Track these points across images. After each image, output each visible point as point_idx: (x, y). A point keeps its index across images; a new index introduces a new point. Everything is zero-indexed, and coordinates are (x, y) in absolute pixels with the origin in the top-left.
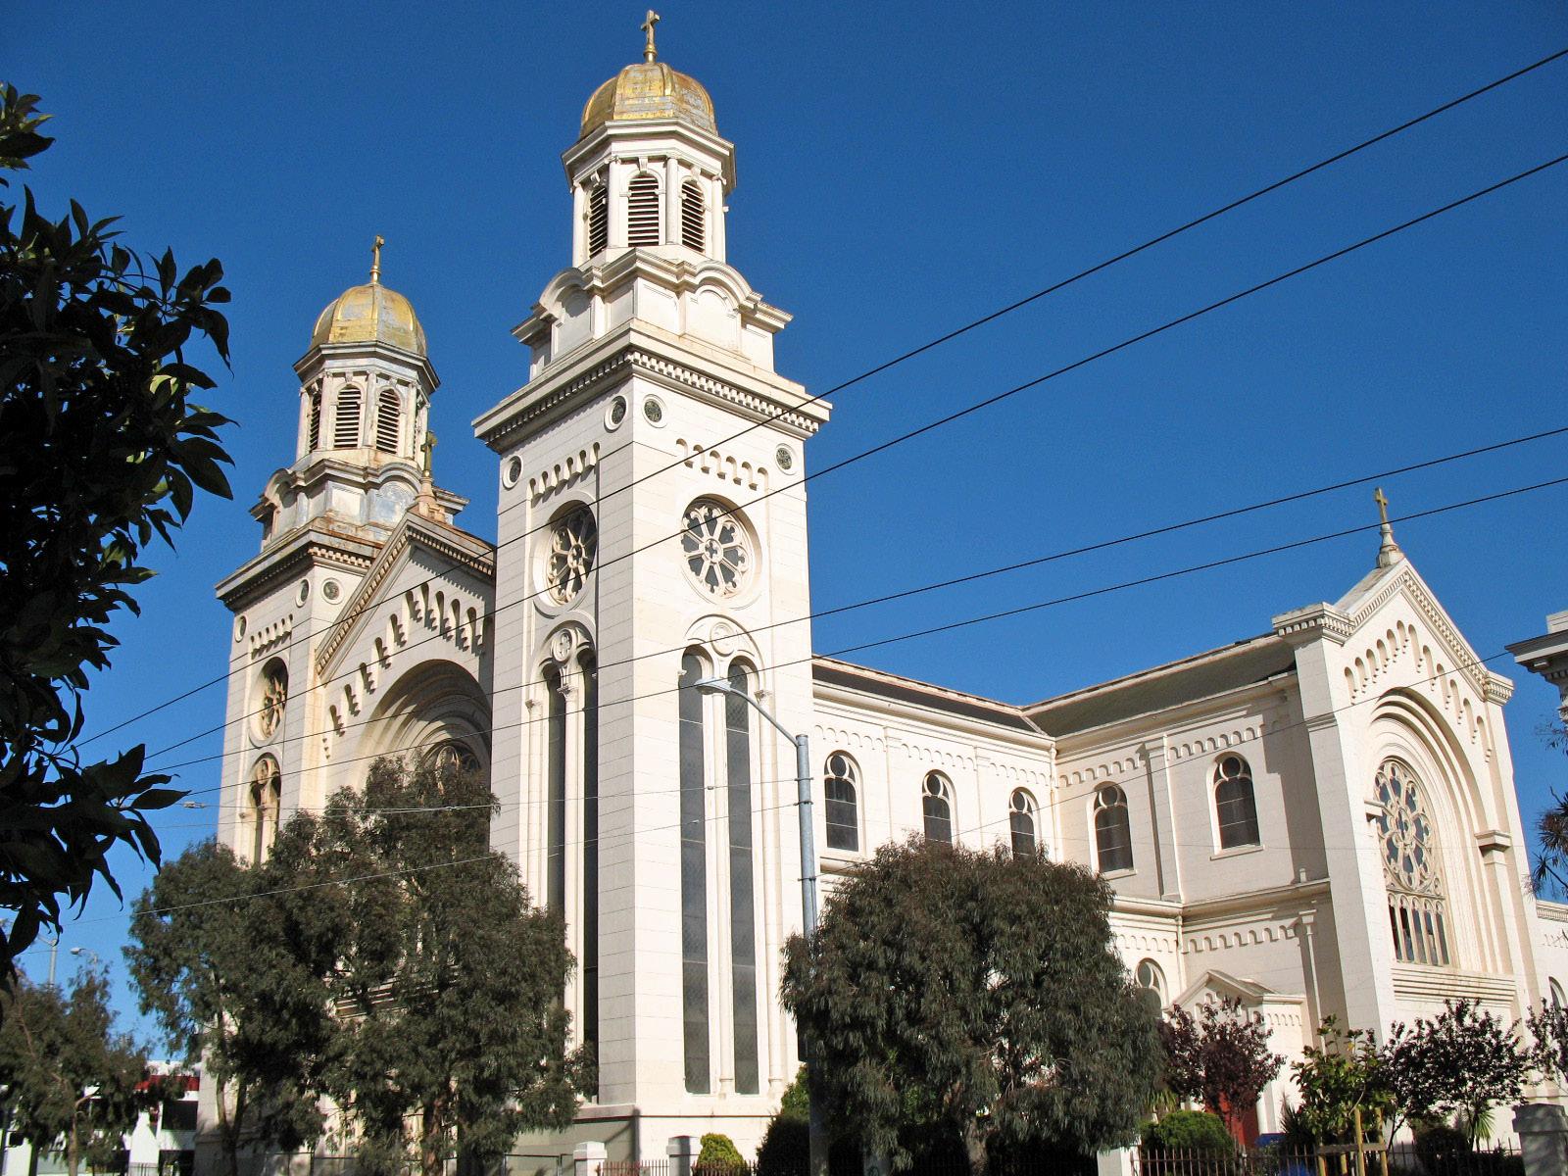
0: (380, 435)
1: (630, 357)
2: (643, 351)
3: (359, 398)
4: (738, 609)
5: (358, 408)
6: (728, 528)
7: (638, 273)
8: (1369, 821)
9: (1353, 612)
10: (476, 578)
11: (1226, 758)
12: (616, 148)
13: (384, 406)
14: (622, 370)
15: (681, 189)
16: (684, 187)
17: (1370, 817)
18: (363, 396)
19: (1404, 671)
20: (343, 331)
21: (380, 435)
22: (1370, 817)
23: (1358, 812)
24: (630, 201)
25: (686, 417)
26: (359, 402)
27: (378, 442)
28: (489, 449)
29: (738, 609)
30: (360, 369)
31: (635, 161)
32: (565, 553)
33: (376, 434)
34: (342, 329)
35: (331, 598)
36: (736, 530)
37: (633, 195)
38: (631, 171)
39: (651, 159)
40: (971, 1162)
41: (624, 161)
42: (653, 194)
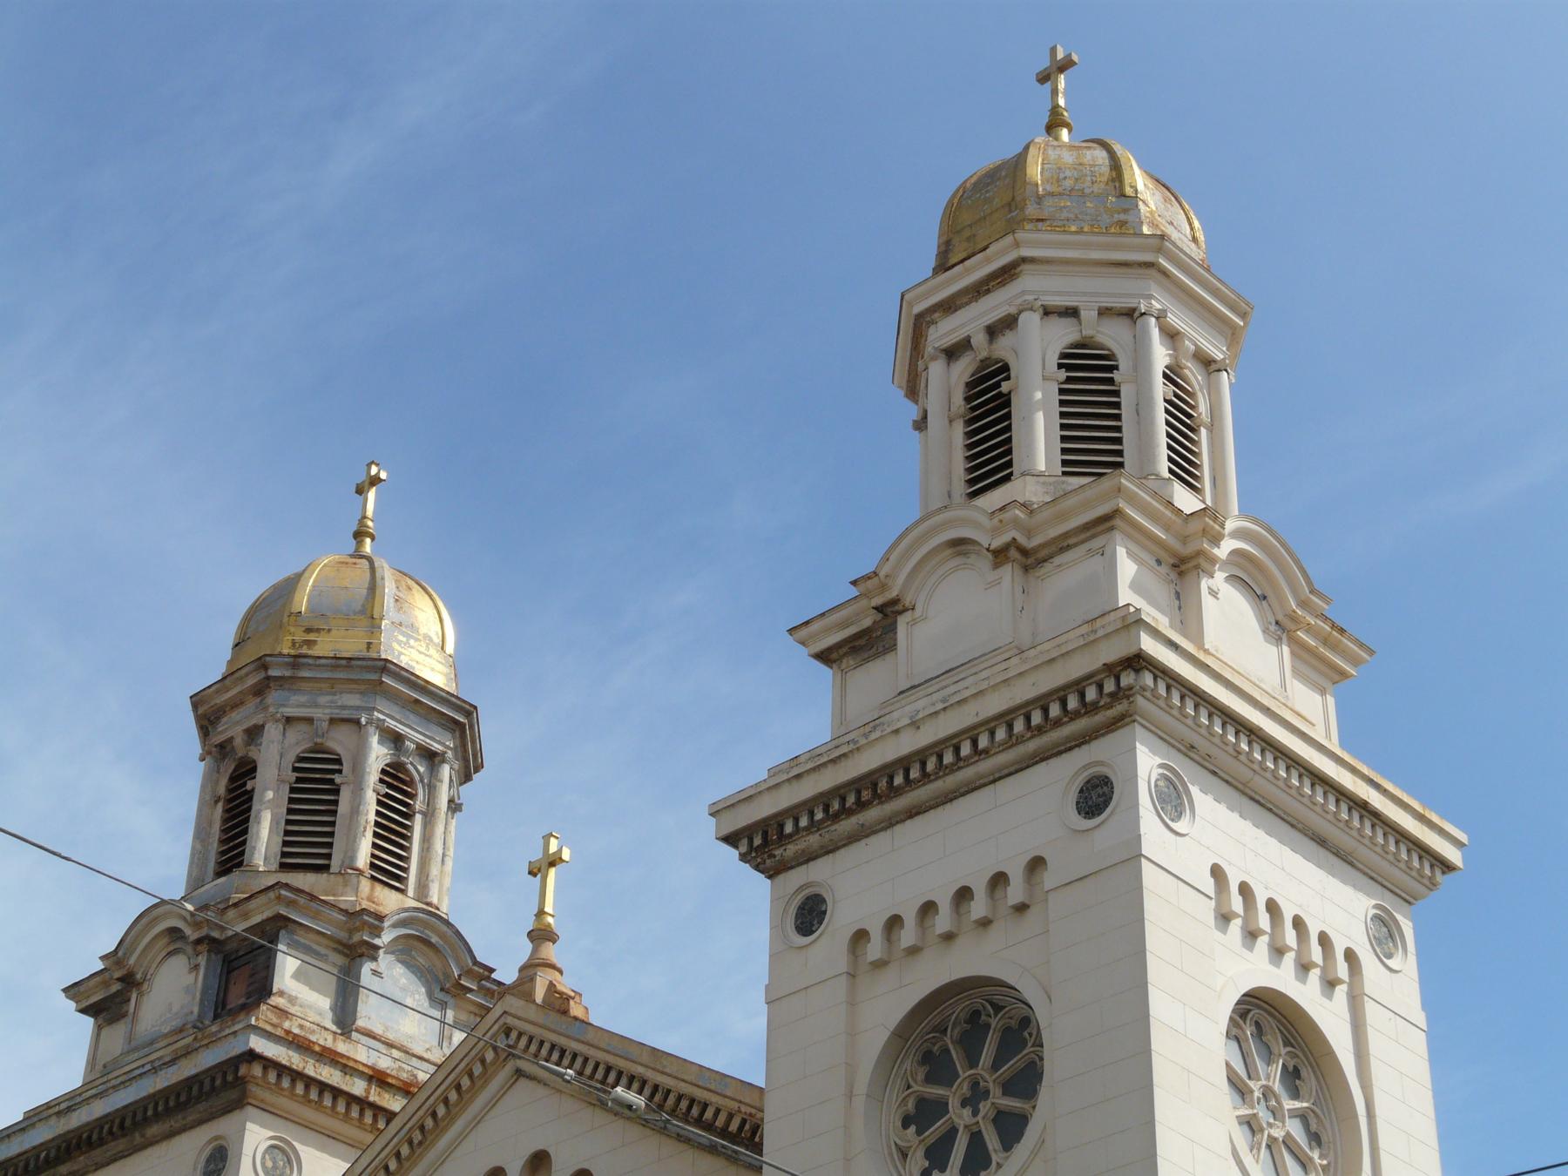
0: (377, 853)
1: (1127, 679)
2: (1161, 672)
3: (340, 771)
5: (337, 792)
6: (913, 1129)
7: (1117, 522)
12: (1030, 284)
13: (387, 795)
14: (1109, 706)
18: (346, 768)
20: (311, 637)
21: (377, 853)
24: (1062, 391)
28: (732, 854)
30: (346, 714)
31: (1072, 313)
32: (937, 1091)
34: (309, 630)
36: (1304, 1073)
38: (1062, 335)
39: (1104, 312)
41: (1047, 312)
42: (331, 781)
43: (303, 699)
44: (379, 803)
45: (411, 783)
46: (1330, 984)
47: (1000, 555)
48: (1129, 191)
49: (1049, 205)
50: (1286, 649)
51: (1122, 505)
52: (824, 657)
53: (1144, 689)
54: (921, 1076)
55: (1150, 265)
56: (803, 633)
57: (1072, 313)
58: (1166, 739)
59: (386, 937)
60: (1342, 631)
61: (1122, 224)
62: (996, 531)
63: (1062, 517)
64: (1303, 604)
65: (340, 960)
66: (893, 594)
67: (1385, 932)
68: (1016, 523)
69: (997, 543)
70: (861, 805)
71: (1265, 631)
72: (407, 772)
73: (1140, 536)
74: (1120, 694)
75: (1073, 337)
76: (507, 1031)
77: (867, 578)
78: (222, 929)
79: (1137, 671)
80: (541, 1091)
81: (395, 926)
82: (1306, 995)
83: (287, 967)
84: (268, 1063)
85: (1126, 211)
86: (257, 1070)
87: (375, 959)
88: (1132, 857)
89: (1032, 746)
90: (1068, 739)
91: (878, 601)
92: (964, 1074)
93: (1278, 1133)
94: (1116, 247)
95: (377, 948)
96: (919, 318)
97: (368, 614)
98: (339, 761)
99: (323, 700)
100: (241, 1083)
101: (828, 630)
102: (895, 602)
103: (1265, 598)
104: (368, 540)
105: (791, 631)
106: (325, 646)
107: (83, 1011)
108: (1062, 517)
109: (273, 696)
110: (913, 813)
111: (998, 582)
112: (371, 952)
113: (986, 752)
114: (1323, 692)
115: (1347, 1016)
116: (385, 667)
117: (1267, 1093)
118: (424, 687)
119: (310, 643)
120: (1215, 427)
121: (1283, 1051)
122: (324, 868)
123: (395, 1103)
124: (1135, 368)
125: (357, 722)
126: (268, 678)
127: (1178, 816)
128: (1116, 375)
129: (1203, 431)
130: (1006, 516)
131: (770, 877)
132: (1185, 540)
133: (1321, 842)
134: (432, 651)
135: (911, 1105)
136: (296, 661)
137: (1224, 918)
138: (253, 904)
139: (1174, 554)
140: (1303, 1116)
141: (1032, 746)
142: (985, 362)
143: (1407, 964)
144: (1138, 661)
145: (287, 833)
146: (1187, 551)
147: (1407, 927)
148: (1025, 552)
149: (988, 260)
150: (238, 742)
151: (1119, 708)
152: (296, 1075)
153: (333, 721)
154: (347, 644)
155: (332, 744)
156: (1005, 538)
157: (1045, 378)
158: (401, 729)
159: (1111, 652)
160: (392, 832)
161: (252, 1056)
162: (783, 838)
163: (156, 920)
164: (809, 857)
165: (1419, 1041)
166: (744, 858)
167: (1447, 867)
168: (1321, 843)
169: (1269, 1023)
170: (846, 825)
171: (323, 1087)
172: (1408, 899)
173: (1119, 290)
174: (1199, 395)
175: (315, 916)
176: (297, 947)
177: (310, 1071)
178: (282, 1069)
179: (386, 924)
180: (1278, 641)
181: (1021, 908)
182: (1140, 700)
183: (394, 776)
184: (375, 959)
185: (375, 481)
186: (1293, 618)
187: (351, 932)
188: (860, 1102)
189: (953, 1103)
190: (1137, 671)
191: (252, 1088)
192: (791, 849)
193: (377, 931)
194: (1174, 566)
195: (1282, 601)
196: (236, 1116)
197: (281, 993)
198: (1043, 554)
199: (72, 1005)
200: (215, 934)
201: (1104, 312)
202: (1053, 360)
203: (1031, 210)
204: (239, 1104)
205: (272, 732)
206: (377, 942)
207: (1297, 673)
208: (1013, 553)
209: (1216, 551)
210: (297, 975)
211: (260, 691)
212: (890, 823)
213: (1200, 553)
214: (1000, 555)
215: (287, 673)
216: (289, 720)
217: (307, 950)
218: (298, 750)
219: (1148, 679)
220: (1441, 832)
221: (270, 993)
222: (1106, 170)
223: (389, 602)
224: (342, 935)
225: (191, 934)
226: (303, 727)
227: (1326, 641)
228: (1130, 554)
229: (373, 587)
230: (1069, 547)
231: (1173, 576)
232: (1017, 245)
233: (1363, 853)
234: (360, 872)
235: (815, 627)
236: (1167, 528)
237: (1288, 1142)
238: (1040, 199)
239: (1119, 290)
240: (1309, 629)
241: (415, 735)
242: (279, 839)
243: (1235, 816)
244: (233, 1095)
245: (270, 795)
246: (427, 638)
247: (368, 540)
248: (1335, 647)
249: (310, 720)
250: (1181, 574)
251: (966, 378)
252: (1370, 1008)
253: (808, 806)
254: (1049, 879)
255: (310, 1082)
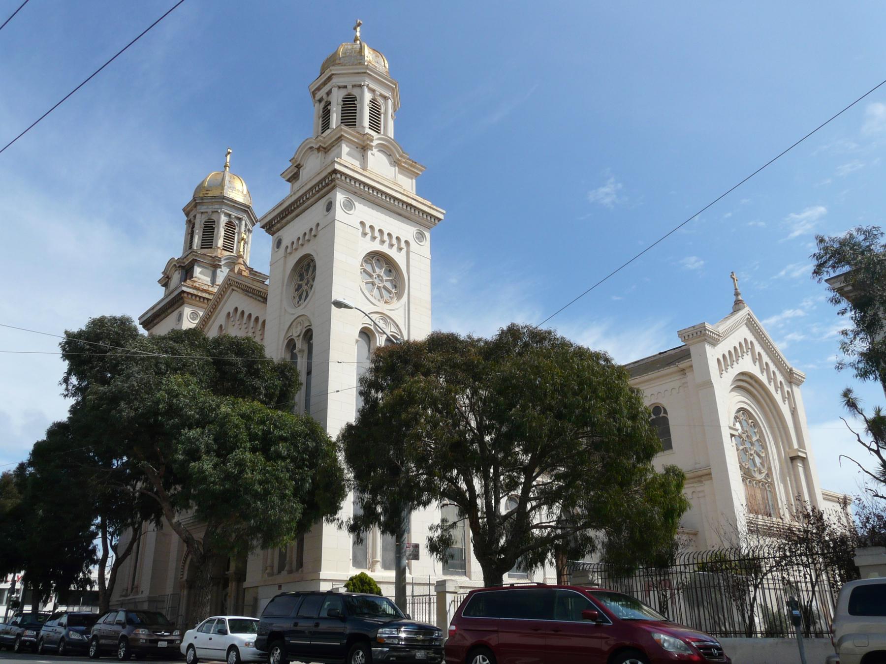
1: (334, 176)
2: (342, 174)
4: (390, 310)
5: (214, 229)
7: (342, 138)
8: (731, 438)
9: (721, 329)
10: (259, 300)
11: (654, 406)
12: (335, 81)
14: (331, 183)
15: (369, 102)
16: (370, 101)
17: (732, 435)
19: (746, 364)
22: (732, 435)
23: (726, 433)
25: (363, 212)
26: (214, 226)
27: (223, 246)
28: (263, 230)
29: (390, 310)
30: (215, 210)
31: (345, 87)
32: (301, 282)
33: (222, 242)
34: (207, 191)
35: (193, 320)
37: (344, 104)
38: (343, 93)
39: (354, 86)
40: (296, 540)
41: (339, 87)
42: (354, 104)
43: (205, 207)
44: (225, 231)
45: (234, 226)
46: (400, 249)
47: (318, 149)
48: (363, 54)
49: (342, 61)
50: (397, 168)
51: (343, 133)
52: (288, 180)
53: (338, 178)
54: (299, 279)
55: (365, 73)
56: (283, 175)
57: (345, 87)
58: (347, 190)
59: (223, 263)
60: (415, 163)
61: (360, 63)
62: (316, 145)
63: (331, 138)
64: (401, 156)
65: (212, 269)
66: (298, 163)
67: (420, 236)
68: (321, 141)
69: (317, 147)
70: (287, 215)
71: (391, 164)
72: (233, 223)
73: (349, 141)
74: (333, 180)
75: (346, 93)
76: (229, 280)
77: (292, 159)
78: (184, 263)
79: (336, 174)
80: (237, 293)
81: (225, 260)
82: (393, 253)
83: (197, 270)
84: (188, 293)
85: (361, 59)
86: (185, 295)
87: (221, 268)
88: (333, 220)
89: (317, 196)
90: (324, 193)
91: (295, 165)
92: (306, 277)
93: (381, 285)
94: (356, 69)
95: (221, 265)
96: (313, 92)
97: (222, 185)
98: (214, 222)
99: (210, 207)
100: (182, 298)
101: (288, 174)
102: (299, 164)
103: (390, 155)
104: (228, 168)
105: (281, 175)
106: (211, 194)
107: (162, 286)
108: (331, 138)
109: (198, 207)
110: (297, 216)
111: (318, 157)
112: (220, 266)
113: (308, 198)
114: (412, 179)
115: (405, 257)
116: (224, 198)
117: (379, 276)
118: (235, 202)
119: (207, 194)
120: (386, 113)
121: (385, 266)
122: (211, 248)
123: (211, 297)
124: (360, 100)
125: (218, 212)
126: (196, 203)
127: (351, 209)
128: (355, 102)
129: (382, 115)
130: (318, 139)
131: (272, 235)
132: (364, 141)
133: (400, 215)
134: (240, 193)
135: (297, 286)
136: (202, 198)
137: (365, 234)
138: (189, 256)
139: (361, 145)
140: (391, 281)
141: (317, 196)
142: (326, 102)
143: (427, 244)
144: (335, 171)
145: (203, 240)
146: (364, 144)
147: (428, 235)
148: (324, 148)
149: (325, 76)
150: (192, 220)
151: (333, 184)
152: (196, 296)
153: (213, 212)
154: (216, 193)
155: (212, 218)
156: (318, 145)
157: (337, 104)
158: (230, 213)
159: (329, 170)
160: (229, 237)
161: (183, 292)
162: (273, 226)
163: (171, 263)
164: (279, 230)
165: (428, 262)
166: (266, 231)
167: (439, 220)
168: (399, 215)
169: (380, 259)
170: (285, 221)
171: (204, 298)
172: (428, 228)
173: (356, 80)
174: (382, 106)
175: (204, 259)
176: (199, 266)
177: (200, 294)
178: (192, 295)
179: (222, 259)
180: (395, 166)
181: (315, 236)
182: (337, 181)
183: (230, 225)
184: (221, 268)
185: (229, 153)
186: (398, 160)
187: (214, 262)
188: (285, 287)
189: (304, 285)
190: (336, 174)
191: (185, 299)
192: (275, 228)
193: (220, 261)
194: (362, 148)
195: (395, 156)
196: (183, 306)
197: (196, 277)
198: (329, 148)
199: (160, 285)
200: (182, 265)
201: (354, 86)
202: (340, 99)
203: (337, 62)
204: (183, 304)
205: (198, 216)
206: (220, 264)
207: (399, 172)
208: (321, 149)
209: (372, 144)
210: (200, 273)
211: (195, 206)
212: (293, 219)
213: (368, 144)
214: (318, 149)
215: (201, 201)
216: (202, 213)
217: (203, 267)
218: (204, 220)
219: (339, 176)
220: (437, 211)
221: (192, 277)
222: (358, 49)
223: (227, 182)
224: (212, 263)
225: (177, 265)
226: (206, 214)
227: (411, 166)
228: (347, 146)
229: (223, 179)
230: (334, 146)
231: (362, 151)
232: (331, 71)
233: (412, 217)
234: (218, 248)
235: (285, 174)
236: (358, 139)
237: (385, 288)
238: (340, 58)
239: (356, 80)
240: (405, 163)
241: (234, 214)
242: (200, 242)
243: (371, 209)
244: (181, 301)
245: (197, 231)
246: (239, 190)
247: (228, 168)
248: (414, 167)
249: (207, 212)
250: (365, 150)
251: (323, 107)
252: (411, 254)
253: (276, 217)
254: (319, 228)
255: (200, 297)
